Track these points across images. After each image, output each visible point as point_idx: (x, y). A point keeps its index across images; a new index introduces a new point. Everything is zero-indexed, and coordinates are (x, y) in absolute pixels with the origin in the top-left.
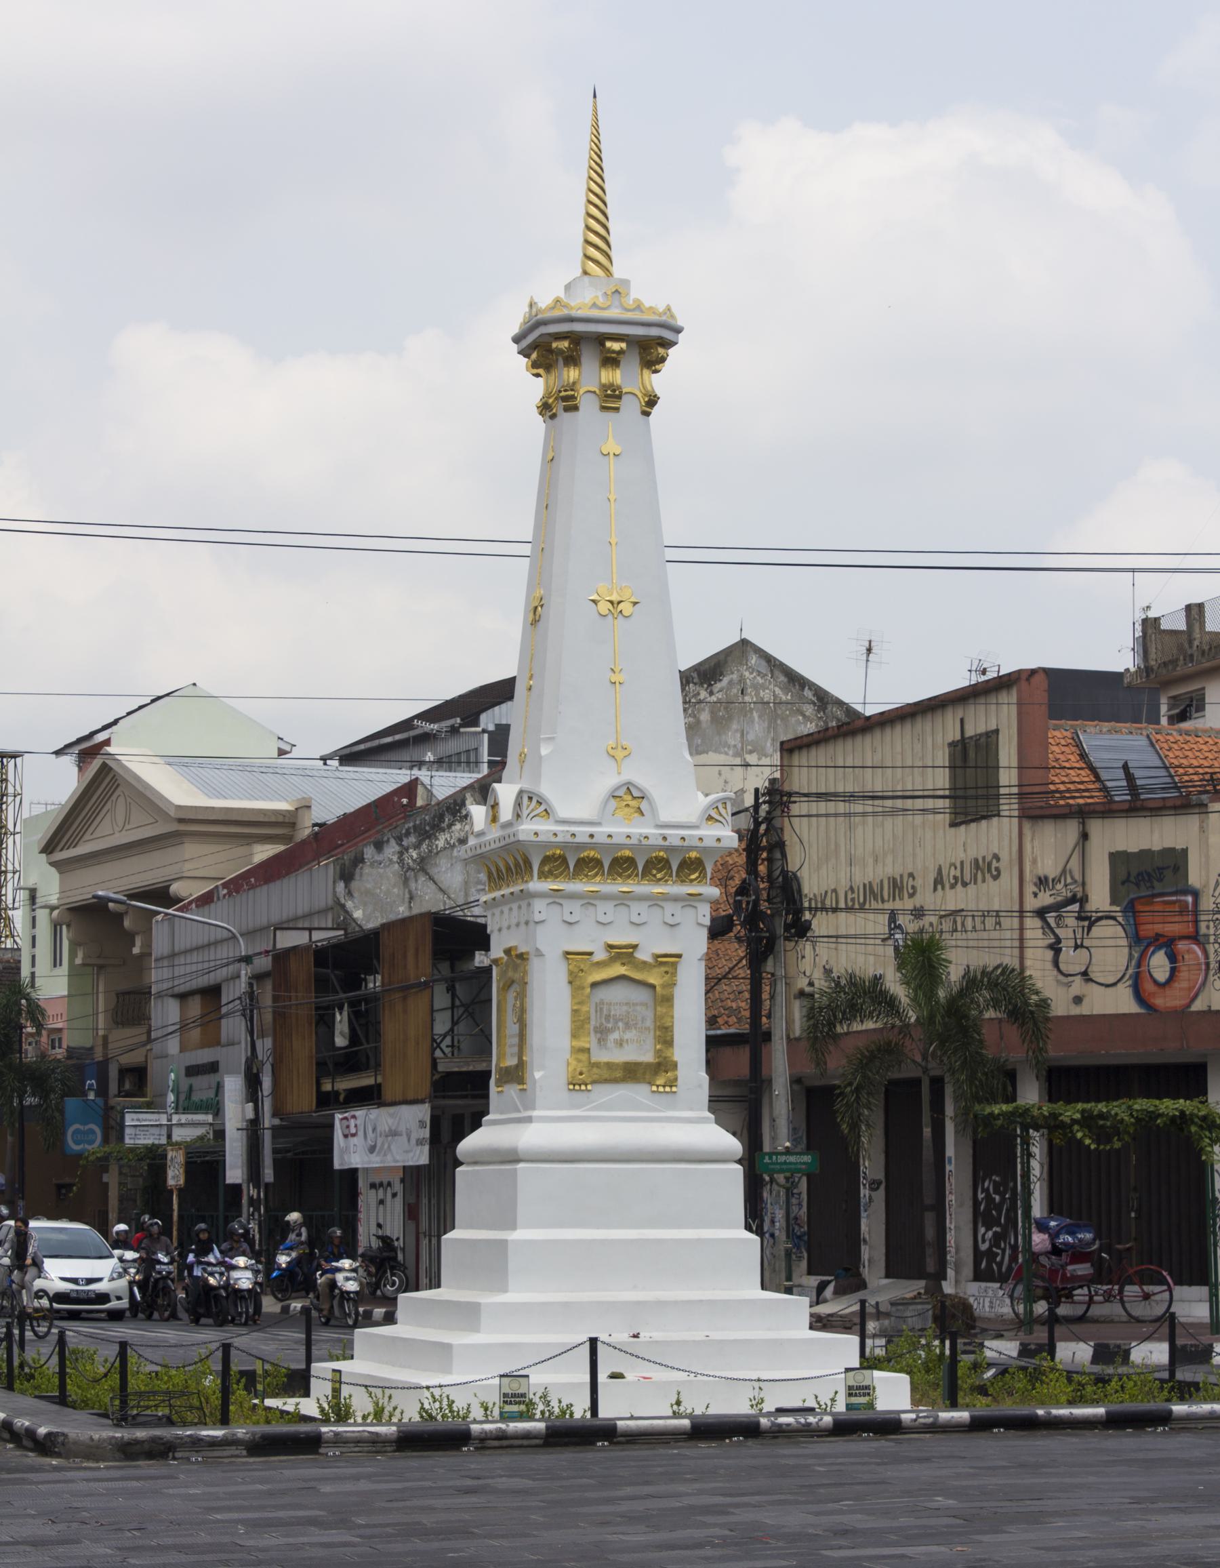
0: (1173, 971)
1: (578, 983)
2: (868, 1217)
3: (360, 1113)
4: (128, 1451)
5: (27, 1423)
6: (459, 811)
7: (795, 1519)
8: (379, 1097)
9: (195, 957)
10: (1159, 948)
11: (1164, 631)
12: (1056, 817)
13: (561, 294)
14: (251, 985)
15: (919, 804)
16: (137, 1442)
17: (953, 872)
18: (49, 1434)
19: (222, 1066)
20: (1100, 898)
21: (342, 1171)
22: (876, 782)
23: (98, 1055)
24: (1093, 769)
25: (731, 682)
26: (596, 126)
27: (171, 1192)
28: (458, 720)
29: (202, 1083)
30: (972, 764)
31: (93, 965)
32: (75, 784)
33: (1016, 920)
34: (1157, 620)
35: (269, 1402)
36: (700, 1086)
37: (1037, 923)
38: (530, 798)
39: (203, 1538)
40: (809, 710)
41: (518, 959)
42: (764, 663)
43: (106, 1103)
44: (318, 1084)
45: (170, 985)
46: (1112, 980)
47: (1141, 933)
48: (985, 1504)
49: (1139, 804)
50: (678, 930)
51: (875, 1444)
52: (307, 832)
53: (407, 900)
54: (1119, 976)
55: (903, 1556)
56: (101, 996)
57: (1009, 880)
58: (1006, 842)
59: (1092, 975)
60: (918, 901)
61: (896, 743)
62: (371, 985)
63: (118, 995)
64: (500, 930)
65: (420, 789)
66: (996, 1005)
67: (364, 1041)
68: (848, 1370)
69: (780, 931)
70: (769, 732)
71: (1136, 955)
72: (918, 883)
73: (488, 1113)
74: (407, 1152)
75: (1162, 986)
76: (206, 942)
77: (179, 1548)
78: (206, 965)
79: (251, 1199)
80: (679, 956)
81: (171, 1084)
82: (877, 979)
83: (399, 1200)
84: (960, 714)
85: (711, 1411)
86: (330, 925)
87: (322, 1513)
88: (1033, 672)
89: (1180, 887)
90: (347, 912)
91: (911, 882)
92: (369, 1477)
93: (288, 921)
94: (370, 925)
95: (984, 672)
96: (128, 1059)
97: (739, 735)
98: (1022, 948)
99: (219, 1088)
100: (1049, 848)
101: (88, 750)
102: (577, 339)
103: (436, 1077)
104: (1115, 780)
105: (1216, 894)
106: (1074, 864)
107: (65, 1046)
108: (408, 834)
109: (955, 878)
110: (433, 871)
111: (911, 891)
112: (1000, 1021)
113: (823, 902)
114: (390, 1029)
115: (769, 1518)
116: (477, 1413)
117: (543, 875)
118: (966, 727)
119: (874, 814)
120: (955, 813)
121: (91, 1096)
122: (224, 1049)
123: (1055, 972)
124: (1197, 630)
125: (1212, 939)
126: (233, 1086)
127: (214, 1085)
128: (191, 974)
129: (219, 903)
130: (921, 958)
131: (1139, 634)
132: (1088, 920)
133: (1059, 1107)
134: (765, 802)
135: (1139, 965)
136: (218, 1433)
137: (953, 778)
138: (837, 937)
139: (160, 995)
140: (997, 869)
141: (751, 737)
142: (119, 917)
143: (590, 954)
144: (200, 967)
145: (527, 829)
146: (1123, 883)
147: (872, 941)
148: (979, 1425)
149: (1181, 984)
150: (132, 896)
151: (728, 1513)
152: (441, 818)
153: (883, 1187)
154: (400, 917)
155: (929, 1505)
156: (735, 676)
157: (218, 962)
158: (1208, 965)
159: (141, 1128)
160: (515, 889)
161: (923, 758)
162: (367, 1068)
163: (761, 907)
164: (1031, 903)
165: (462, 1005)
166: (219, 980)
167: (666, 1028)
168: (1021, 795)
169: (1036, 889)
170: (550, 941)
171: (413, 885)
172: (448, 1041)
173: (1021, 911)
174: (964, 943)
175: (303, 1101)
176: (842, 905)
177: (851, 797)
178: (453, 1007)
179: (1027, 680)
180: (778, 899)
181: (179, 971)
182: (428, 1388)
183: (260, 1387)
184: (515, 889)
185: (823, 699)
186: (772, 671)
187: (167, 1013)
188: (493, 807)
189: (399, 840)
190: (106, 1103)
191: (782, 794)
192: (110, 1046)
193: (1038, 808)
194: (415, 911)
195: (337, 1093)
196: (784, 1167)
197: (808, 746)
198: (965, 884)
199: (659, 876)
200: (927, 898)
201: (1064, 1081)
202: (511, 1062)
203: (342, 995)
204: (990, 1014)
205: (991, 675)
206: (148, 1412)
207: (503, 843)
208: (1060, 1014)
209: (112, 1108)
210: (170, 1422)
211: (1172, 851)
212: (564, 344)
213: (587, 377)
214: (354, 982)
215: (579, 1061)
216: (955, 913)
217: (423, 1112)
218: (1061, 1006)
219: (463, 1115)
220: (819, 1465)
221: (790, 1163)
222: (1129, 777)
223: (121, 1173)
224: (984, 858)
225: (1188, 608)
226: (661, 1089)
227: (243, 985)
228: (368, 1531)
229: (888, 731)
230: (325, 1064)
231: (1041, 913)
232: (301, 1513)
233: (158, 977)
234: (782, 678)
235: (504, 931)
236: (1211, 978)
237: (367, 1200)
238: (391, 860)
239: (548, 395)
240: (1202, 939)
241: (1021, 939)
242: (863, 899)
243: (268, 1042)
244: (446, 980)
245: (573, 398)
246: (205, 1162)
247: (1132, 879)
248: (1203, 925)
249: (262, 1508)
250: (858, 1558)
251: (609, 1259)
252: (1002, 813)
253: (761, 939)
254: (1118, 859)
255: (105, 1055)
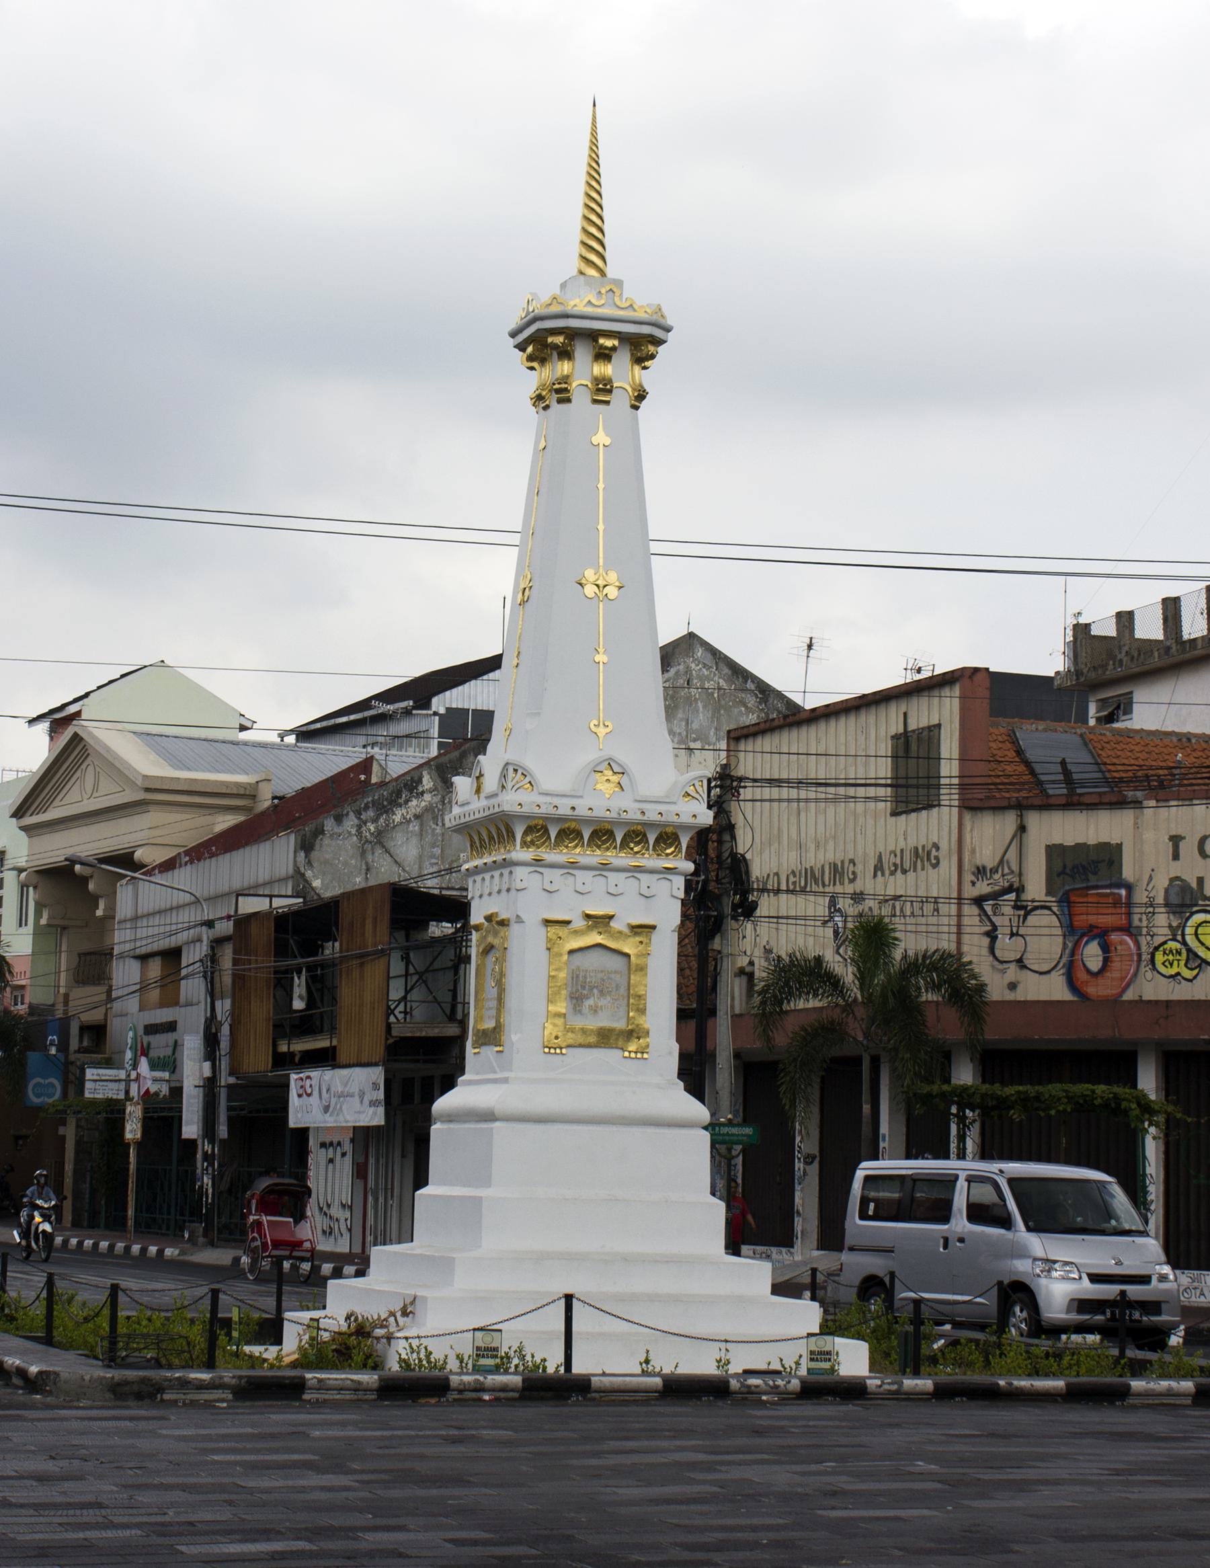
0: (1106, 961)
1: (556, 950)
2: (802, 1190)
3: (315, 1074)
4: (119, 1392)
5: (18, 1362)
6: (416, 788)
7: (782, 1477)
8: (334, 1059)
9: (156, 920)
10: (1093, 938)
11: (1094, 636)
12: (994, 809)
13: (557, 291)
14: (212, 948)
15: (861, 791)
16: (126, 1383)
17: (892, 859)
18: (40, 1373)
19: (179, 1026)
20: (1036, 888)
21: (293, 1129)
22: (818, 769)
23: (59, 1014)
24: (1027, 763)
25: (677, 673)
26: (594, 133)
27: (129, 1144)
28: (411, 703)
29: (161, 1043)
30: (913, 753)
31: (57, 926)
32: (46, 754)
33: (954, 908)
34: (1087, 626)
35: (247, 1349)
36: (670, 1053)
37: (975, 910)
38: (516, 771)
39: (205, 1479)
40: (751, 701)
41: (498, 923)
42: (709, 656)
43: (67, 1057)
44: (275, 1046)
45: (132, 946)
46: (1046, 968)
47: (1076, 923)
48: (967, 1471)
49: (1075, 799)
50: (654, 898)
51: (843, 1408)
52: (267, 804)
53: (363, 871)
54: (1053, 964)
55: (897, 1519)
56: (64, 955)
57: (948, 868)
58: (945, 833)
59: (1026, 962)
60: (858, 886)
61: (840, 733)
62: (327, 952)
63: (79, 955)
64: (481, 896)
65: (375, 767)
66: (936, 987)
67: (319, 1004)
68: (810, 1335)
69: (728, 910)
70: (712, 722)
71: (1070, 945)
72: (859, 868)
73: (463, 1073)
74: (359, 1112)
75: (1095, 975)
76: (168, 906)
77: (183, 1488)
78: (168, 928)
79: (205, 1154)
80: (654, 927)
81: (129, 1041)
82: (819, 960)
83: (348, 1159)
84: (903, 708)
85: (680, 1371)
86: (290, 893)
87: (312, 1457)
88: (976, 670)
89: (1114, 880)
90: (306, 881)
91: (851, 868)
92: (355, 1424)
93: (249, 888)
94: (327, 894)
95: (919, 671)
96: (95, 1016)
97: (684, 723)
98: (959, 933)
99: (176, 1045)
100: (989, 836)
101: (59, 720)
102: (573, 335)
103: (391, 1041)
104: (1050, 773)
105: (1149, 888)
106: (1012, 855)
107: (27, 1000)
108: (366, 808)
109: (895, 865)
110: (390, 844)
111: (851, 877)
112: (937, 1003)
113: (765, 883)
114: (346, 993)
115: (755, 1474)
116: (453, 1365)
117: (525, 844)
118: (909, 721)
119: (817, 800)
120: (896, 800)
121: (53, 1051)
122: (183, 1009)
123: (991, 958)
124: (1127, 635)
125: (1144, 931)
126: (192, 1044)
127: (171, 1043)
128: (153, 936)
129: (183, 869)
130: (872, 938)
131: (1070, 638)
132: (1024, 909)
133: (997, 1089)
134: (716, 786)
135: (1073, 954)
136: (205, 1376)
137: (895, 768)
138: (778, 917)
139: (122, 956)
140: (937, 858)
141: (695, 726)
142: (84, 880)
143: (568, 922)
144: (162, 930)
145: (510, 801)
146: (1059, 875)
147: (812, 923)
148: (943, 1393)
149: (1114, 973)
150: (103, 860)
151: (715, 1471)
152: (399, 794)
153: (817, 1160)
154: (357, 887)
155: (911, 1469)
156: (681, 667)
157: (180, 926)
158: (1139, 955)
159: (99, 1084)
160: (498, 857)
161: (865, 750)
162: (321, 1031)
163: (719, 887)
164: (970, 892)
165: (417, 973)
166: (179, 943)
167: (640, 996)
168: (962, 786)
169: (973, 878)
170: (531, 913)
171: (370, 858)
172: (401, 1008)
173: (959, 898)
174: (913, 928)
175: (258, 1061)
176: (784, 887)
177: (800, 783)
178: (407, 975)
179: (970, 677)
180: (727, 880)
181: (141, 933)
182: (406, 1338)
183: (235, 1334)
184: (498, 857)
185: (765, 691)
186: (717, 664)
187: (125, 974)
188: (478, 778)
189: (358, 813)
190: (67, 1057)
191: (732, 779)
192: (71, 1004)
193: (976, 800)
194: (372, 883)
195: (292, 1055)
196: (727, 1138)
197: (754, 735)
198: (904, 872)
199: (636, 849)
200: (866, 884)
201: (993, 1062)
202: (490, 1024)
203: (301, 960)
204: (930, 997)
205: (926, 674)
206: (136, 1354)
207: (487, 813)
208: (995, 999)
209: (72, 1063)
210: (158, 1365)
211: (1106, 845)
212: (559, 340)
213: (581, 370)
214: (311, 948)
215: (555, 1025)
216: (896, 898)
217: (377, 1074)
218: (996, 990)
219: (432, 1077)
220: (793, 1427)
221: (733, 1135)
222: (1066, 772)
223: (78, 1126)
224: (923, 847)
225: (1119, 615)
226: (633, 1055)
227: (205, 948)
228: (365, 1477)
229: (833, 722)
230: (282, 1026)
231: (979, 901)
232: (295, 1457)
233: (121, 939)
234: (726, 671)
235: (485, 897)
236: (1142, 969)
237: (317, 1159)
238: (349, 833)
239: (542, 386)
240: (1133, 931)
241: (959, 925)
242: (805, 882)
243: (228, 1003)
244: (401, 949)
245: (566, 390)
246: (162, 1115)
247: (1068, 871)
248: (1136, 918)
249: (258, 1451)
250: (852, 1519)
251: (570, 1217)
252: (942, 803)
253: (710, 917)
254: (1053, 851)
255: (66, 1012)
